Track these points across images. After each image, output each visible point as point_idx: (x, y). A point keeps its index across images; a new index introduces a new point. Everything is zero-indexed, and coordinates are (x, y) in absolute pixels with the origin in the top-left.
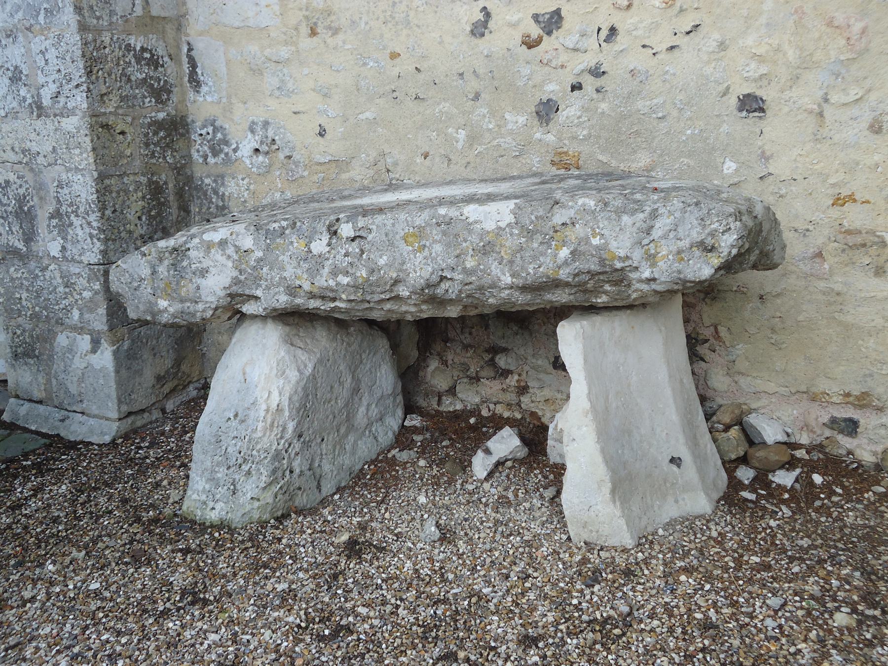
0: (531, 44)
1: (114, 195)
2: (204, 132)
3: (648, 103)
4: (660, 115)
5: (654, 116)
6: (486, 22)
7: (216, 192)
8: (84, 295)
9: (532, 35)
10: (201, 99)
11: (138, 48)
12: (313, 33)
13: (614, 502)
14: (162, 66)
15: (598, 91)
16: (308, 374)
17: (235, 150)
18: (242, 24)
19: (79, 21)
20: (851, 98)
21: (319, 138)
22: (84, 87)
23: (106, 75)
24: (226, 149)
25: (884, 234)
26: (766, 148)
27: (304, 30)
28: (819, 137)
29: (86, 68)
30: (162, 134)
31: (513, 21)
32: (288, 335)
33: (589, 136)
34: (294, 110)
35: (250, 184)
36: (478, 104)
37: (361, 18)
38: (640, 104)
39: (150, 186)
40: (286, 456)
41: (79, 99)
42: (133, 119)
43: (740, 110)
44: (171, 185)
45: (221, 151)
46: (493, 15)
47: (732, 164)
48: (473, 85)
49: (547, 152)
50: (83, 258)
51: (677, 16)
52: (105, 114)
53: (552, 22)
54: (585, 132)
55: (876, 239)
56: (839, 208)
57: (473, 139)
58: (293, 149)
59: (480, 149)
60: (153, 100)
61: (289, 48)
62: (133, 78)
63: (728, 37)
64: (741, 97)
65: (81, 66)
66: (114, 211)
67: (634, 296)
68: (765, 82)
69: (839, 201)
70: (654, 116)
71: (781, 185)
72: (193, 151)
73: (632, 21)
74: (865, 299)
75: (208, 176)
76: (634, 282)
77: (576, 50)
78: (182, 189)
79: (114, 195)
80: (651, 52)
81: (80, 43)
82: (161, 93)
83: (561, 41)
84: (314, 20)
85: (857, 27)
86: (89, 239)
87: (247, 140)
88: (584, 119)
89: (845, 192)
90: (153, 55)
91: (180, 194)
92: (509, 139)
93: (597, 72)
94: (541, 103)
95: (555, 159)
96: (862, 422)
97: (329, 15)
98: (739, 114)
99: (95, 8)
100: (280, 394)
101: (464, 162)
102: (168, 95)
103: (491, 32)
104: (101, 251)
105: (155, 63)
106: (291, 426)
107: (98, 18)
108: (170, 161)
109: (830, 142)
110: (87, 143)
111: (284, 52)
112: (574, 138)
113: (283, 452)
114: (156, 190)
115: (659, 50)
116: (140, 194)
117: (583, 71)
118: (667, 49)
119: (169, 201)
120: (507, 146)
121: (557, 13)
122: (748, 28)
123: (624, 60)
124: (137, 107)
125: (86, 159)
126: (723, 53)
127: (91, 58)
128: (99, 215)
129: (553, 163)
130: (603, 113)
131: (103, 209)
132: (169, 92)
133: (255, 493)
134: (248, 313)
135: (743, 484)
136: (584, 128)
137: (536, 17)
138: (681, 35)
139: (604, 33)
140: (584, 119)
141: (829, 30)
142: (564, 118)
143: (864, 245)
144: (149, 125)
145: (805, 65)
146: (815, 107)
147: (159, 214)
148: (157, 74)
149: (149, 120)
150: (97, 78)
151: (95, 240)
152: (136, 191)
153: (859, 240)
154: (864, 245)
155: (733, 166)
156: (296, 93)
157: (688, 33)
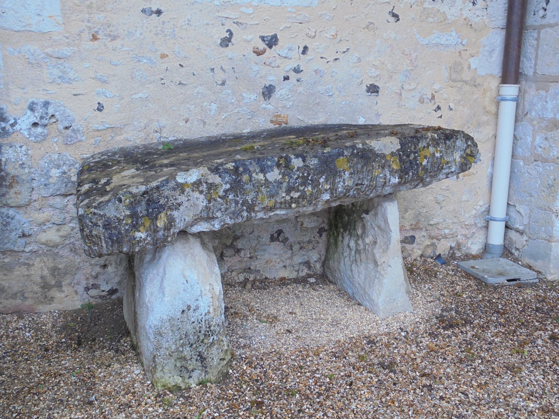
0: (259, 53)
3: (323, 88)
4: (330, 94)
6: (230, 38)
9: (259, 48)
12: (95, 38)
15: (298, 81)
17: (13, 125)
18: (24, 29)
20: (412, 87)
21: (97, 112)
27: (87, 36)
31: (247, 39)
33: (293, 105)
34: (73, 93)
35: (28, 150)
37: (136, 30)
38: (320, 88)
43: (368, 92)
46: (234, 35)
48: (220, 76)
49: (269, 115)
51: (338, 43)
53: (272, 42)
54: (291, 103)
57: (221, 109)
58: (73, 121)
64: (368, 85)
68: (378, 79)
73: (316, 44)
77: (285, 57)
80: (326, 61)
84: (96, 29)
85: (414, 55)
87: (26, 117)
92: (245, 108)
93: (297, 70)
95: (273, 119)
96: (416, 236)
97: (108, 26)
101: (215, 123)
109: (404, 107)
111: (66, 51)
117: (291, 69)
120: (244, 112)
123: (309, 64)
126: (359, 63)
129: (272, 122)
130: (300, 93)
135: (50, 285)
136: (290, 101)
137: (263, 38)
139: (301, 49)
141: (403, 56)
142: (279, 96)
156: (77, 81)
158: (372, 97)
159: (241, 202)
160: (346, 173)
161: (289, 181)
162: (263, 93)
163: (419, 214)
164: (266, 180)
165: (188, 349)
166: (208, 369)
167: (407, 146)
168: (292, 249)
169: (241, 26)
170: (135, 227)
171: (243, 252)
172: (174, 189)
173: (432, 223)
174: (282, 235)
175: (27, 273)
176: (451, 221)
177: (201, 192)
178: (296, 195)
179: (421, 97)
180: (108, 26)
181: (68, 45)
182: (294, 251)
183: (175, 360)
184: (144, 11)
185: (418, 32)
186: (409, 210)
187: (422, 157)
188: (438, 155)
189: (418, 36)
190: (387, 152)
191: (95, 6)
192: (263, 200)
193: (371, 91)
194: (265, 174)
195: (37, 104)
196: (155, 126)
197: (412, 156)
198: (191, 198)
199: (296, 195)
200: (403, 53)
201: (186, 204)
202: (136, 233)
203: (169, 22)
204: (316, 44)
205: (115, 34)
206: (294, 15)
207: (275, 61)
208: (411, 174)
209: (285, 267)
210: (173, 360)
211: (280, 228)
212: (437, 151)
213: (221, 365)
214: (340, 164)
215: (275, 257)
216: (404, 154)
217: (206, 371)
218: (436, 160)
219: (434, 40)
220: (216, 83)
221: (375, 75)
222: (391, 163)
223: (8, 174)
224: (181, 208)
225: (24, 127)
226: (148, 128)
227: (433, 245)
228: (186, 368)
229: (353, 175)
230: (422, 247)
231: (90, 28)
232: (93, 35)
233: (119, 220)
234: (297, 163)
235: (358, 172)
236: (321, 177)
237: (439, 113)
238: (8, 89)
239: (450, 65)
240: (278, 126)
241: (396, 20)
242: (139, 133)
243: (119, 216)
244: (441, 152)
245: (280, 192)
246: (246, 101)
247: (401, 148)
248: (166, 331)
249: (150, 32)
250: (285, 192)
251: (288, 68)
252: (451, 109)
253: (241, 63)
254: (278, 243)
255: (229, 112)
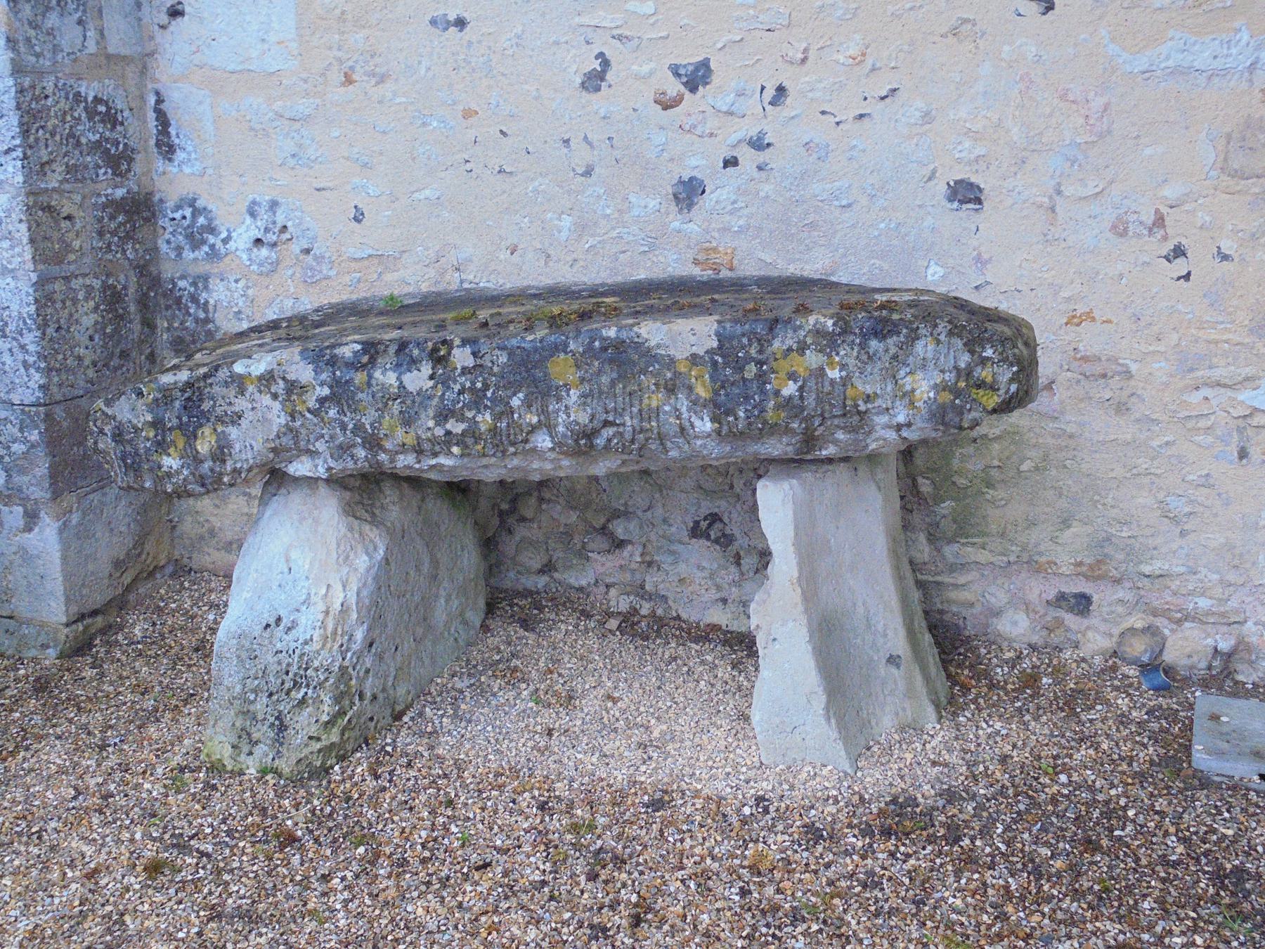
0: (667, 104)
1: (59, 305)
2: (178, 215)
4: (844, 202)
5: (836, 203)
6: (604, 72)
7: (194, 299)
8: (13, 450)
9: (669, 92)
10: (175, 170)
11: (90, 99)
13: (828, 719)
14: (122, 124)
15: (760, 168)
16: (379, 558)
17: (226, 241)
19: (12, 59)
22: (19, 153)
23: (48, 136)
24: (211, 239)
25: (1128, 362)
26: (983, 249)
27: (336, 76)
28: (1049, 237)
29: (21, 124)
30: (121, 218)
31: (642, 73)
32: (348, 504)
33: (748, 227)
34: (315, 185)
35: (248, 287)
36: (590, 181)
37: (420, 63)
38: (816, 188)
39: (104, 292)
40: (354, 674)
41: (10, 169)
42: (84, 198)
44: (131, 291)
45: (204, 242)
46: (613, 63)
47: (939, 269)
48: (581, 156)
49: (689, 247)
50: (12, 396)
51: (868, 75)
52: (47, 190)
53: (697, 77)
54: (741, 222)
55: (1119, 368)
56: (1074, 328)
57: (582, 228)
58: (315, 238)
59: (592, 241)
60: (109, 171)
61: (311, 100)
62: (84, 140)
63: (934, 106)
64: (952, 183)
65: (16, 124)
66: (58, 329)
67: (873, 446)
69: (1074, 320)
70: (836, 203)
71: (1001, 297)
72: (160, 242)
73: (807, 79)
74: (1104, 443)
75: (183, 277)
76: (878, 428)
78: (145, 295)
79: (59, 305)
80: (833, 120)
81: (13, 89)
82: (119, 161)
83: (710, 101)
84: (350, 63)
86: (22, 370)
87: (244, 227)
88: (740, 204)
89: (1081, 309)
90: (109, 109)
91: (143, 302)
93: (759, 144)
94: (681, 182)
96: (1095, 598)
97: (372, 56)
98: (949, 205)
99: (34, 41)
100: (344, 586)
101: (569, 259)
102: (129, 165)
103: (610, 86)
104: (41, 387)
105: (112, 119)
106: (359, 635)
107: (38, 55)
108: (131, 257)
109: (1063, 245)
110: (23, 232)
111: (303, 106)
112: (725, 230)
113: (350, 670)
114: (113, 298)
115: (844, 118)
116: (92, 303)
117: (740, 141)
118: (855, 118)
119: (129, 313)
120: (631, 238)
121: (705, 64)
122: (960, 96)
123: (790, 130)
124: (89, 181)
125: (19, 255)
126: (928, 127)
127: (28, 112)
128: (38, 334)
129: (696, 262)
130: (767, 197)
131: (43, 327)
132: (131, 160)
133: (313, 730)
134: (298, 474)
136: (740, 217)
137: (675, 71)
138: (874, 101)
139: (770, 93)
140: (740, 204)
141: (1062, 105)
143: (1104, 376)
144: (104, 207)
145: (1033, 147)
146: (1046, 200)
147: (116, 331)
148: (115, 135)
149: (104, 199)
150: (37, 140)
151: (32, 371)
152: (86, 299)
153: (1098, 369)
154: (1104, 376)
155: (941, 271)
157: (882, 98)
158: (961, 214)
159: (351, 426)
160: (572, 392)
161: (443, 394)
162: (676, 196)
163: (1109, 539)
164: (401, 386)
165: (265, 700)
166: (284, 750)
167: (735, 343)
168: (738, 564)
169: (629, 44)
170: (161, 446)
171: (630, 547)
172: (227, 384)
173: (1147, 569)
174: (718, 525)
175: (246, 510)
176: (1216, 577)
177: (275, 396)
178: (457, 428)
179: (1119, 218)
180: (372, 56)
181: (307, 94)
182: (745, 568)
183: (237, 715)
184: (433, 22)
185: (1113, 40)
186: (1075, 523)
187: (782, 375)
188: (834, 374)
189: (1113, 48)
190: (680, 353)
191: (350, 17)
192: (392, 428)
193: (959, 197)
194: (400, 374)
195: (259, 204)
196: (452, 258)
197: (751, 370)
198: (258, 406)
199: (457, 428)
200: (1063, 97)
201: (249, 415)
202: (165, 457)
203: (479, 42)
204: (807, 79)
205: (383, 70)
206: (751, 12)
207: (704, 121)
208: (741, 414)
209: (724, 601)
210: (232, 713)
211: (716, 510)
212: (831, 364)
213: (310, 749)
214: (558, 369)
215: (699, 574)
216: (726, 364)
217: (279, 752)
218: (827, 388)
219: (1168, 58)
220: (574, 170)
221: (972, 156)
222: (693, 380)
223: (218, 329)
224: (244, 422)
225: (242, 246)
226: (443, 260)
227: (1150, 630)
228: (249, 734)
229: (589, 400)
230: (1116, 631)
231: (340, 61)
232: (346, 75)
233: (137, 430)
234: (462, 357)
235: (601, 393)
236: (515, 394)
237: (1180, 266)
238: (220, 176)
239: (1227, 129)
240: (710, 272)
241: (1042, 10)
242: (426, 270)
243: (135, 421)
244: (843, 367)
245: (423, 416)
246: (635, 212)
247: (720, 347)
248: (228, 655)
249: (445, 64)
250: (434, 418)
251: (734, 138)
252: (1225, 258)
253: (628, 128)
254: (709, 544)
255: (599, 235)
